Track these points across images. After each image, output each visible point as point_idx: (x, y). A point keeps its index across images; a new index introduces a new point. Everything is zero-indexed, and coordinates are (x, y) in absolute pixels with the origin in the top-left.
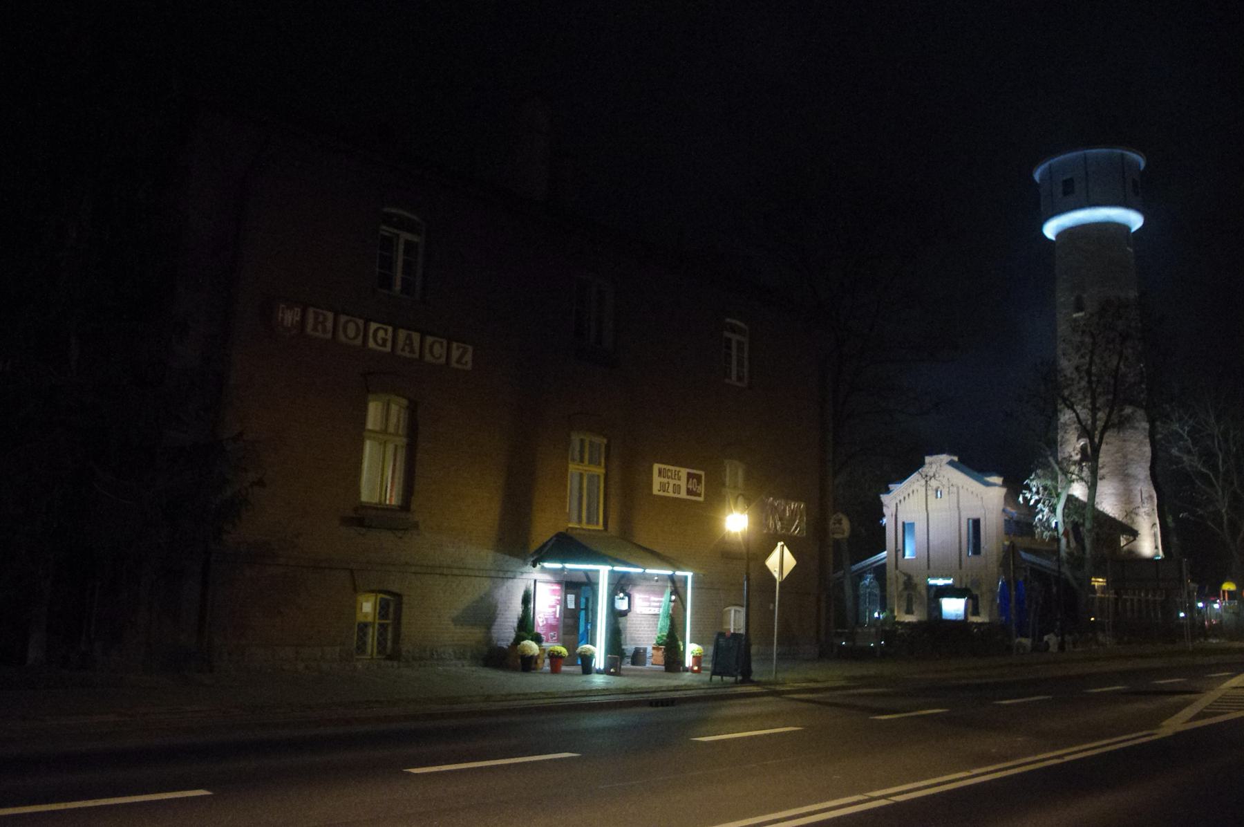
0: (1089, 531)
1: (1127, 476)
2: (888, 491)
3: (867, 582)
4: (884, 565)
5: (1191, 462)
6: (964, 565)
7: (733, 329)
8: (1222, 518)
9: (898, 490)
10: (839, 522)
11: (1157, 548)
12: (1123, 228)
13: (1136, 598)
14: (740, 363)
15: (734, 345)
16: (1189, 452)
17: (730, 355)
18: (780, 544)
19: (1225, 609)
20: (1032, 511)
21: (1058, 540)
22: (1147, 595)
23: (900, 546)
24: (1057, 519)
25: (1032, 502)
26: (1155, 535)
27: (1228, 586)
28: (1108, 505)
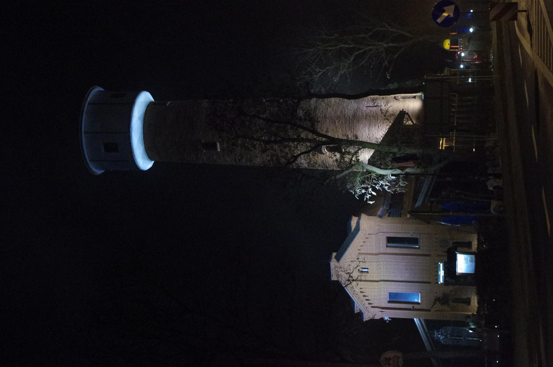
0: (400, 150)
2: (360, 314)
4: (426, 321)
6: (427, 280)
9: (359, 305)
11: (415, 97)
12: (150, 107)
19: (465, 49)
22: (454, 107)
23: (410, 306)
25: (374, 193)
27: (447, 45)
28: (378, 133)
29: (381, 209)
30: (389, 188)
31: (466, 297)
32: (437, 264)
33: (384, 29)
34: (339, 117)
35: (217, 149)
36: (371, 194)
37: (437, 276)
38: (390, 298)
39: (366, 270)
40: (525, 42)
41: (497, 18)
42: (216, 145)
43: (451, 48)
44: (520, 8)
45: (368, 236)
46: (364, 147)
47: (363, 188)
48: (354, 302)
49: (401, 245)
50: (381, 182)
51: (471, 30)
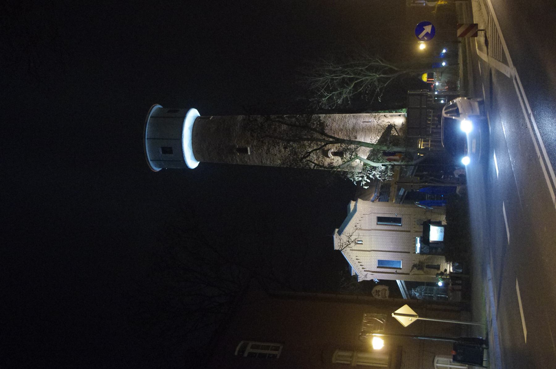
0: (388, 148)
1: (353, 128)
2: (356, 277)
3: (417, 294)
4: (405, 282)
5: (347, 92)
6: (407, 251)
7: (242, 351)
8: (381, 77)
9: (355, 269)
10: (378, 292)
11: (400, 115)
12: (197, 121)
13: (432, 126)
14: (267, 348)
15: (252, 351)
16: (341, 94)
17: (260, 354)
18: (393, 315)
19: (439, 80)
20: (374, 182)
21: (393, 166)
22: (430, 120)
23: (394, 271)
24: (379, 166)
25: (368, 181)
26: (391, 116)
27: (425, 78)
28: (373, 139)
29: (373, 195)
30: (380, 177)
31: (436, 264)
32: (415, 238)
33: (378, 64)
34: (342, 130)
35: (247, 152)
36: (366, 181)
37: (415, 247)
38: (379, 264)
39: (361, 242)
40: (483, 56)
41: (463, 35)
42: (247, 149)
43: (428, 81)
44: (479, 28)
45: (363, 216)
46: (361, 146)
47: (361, 177)
48: (351, 267)
49: (389, 224)
50: (374, 172)
51: (444, 64)
